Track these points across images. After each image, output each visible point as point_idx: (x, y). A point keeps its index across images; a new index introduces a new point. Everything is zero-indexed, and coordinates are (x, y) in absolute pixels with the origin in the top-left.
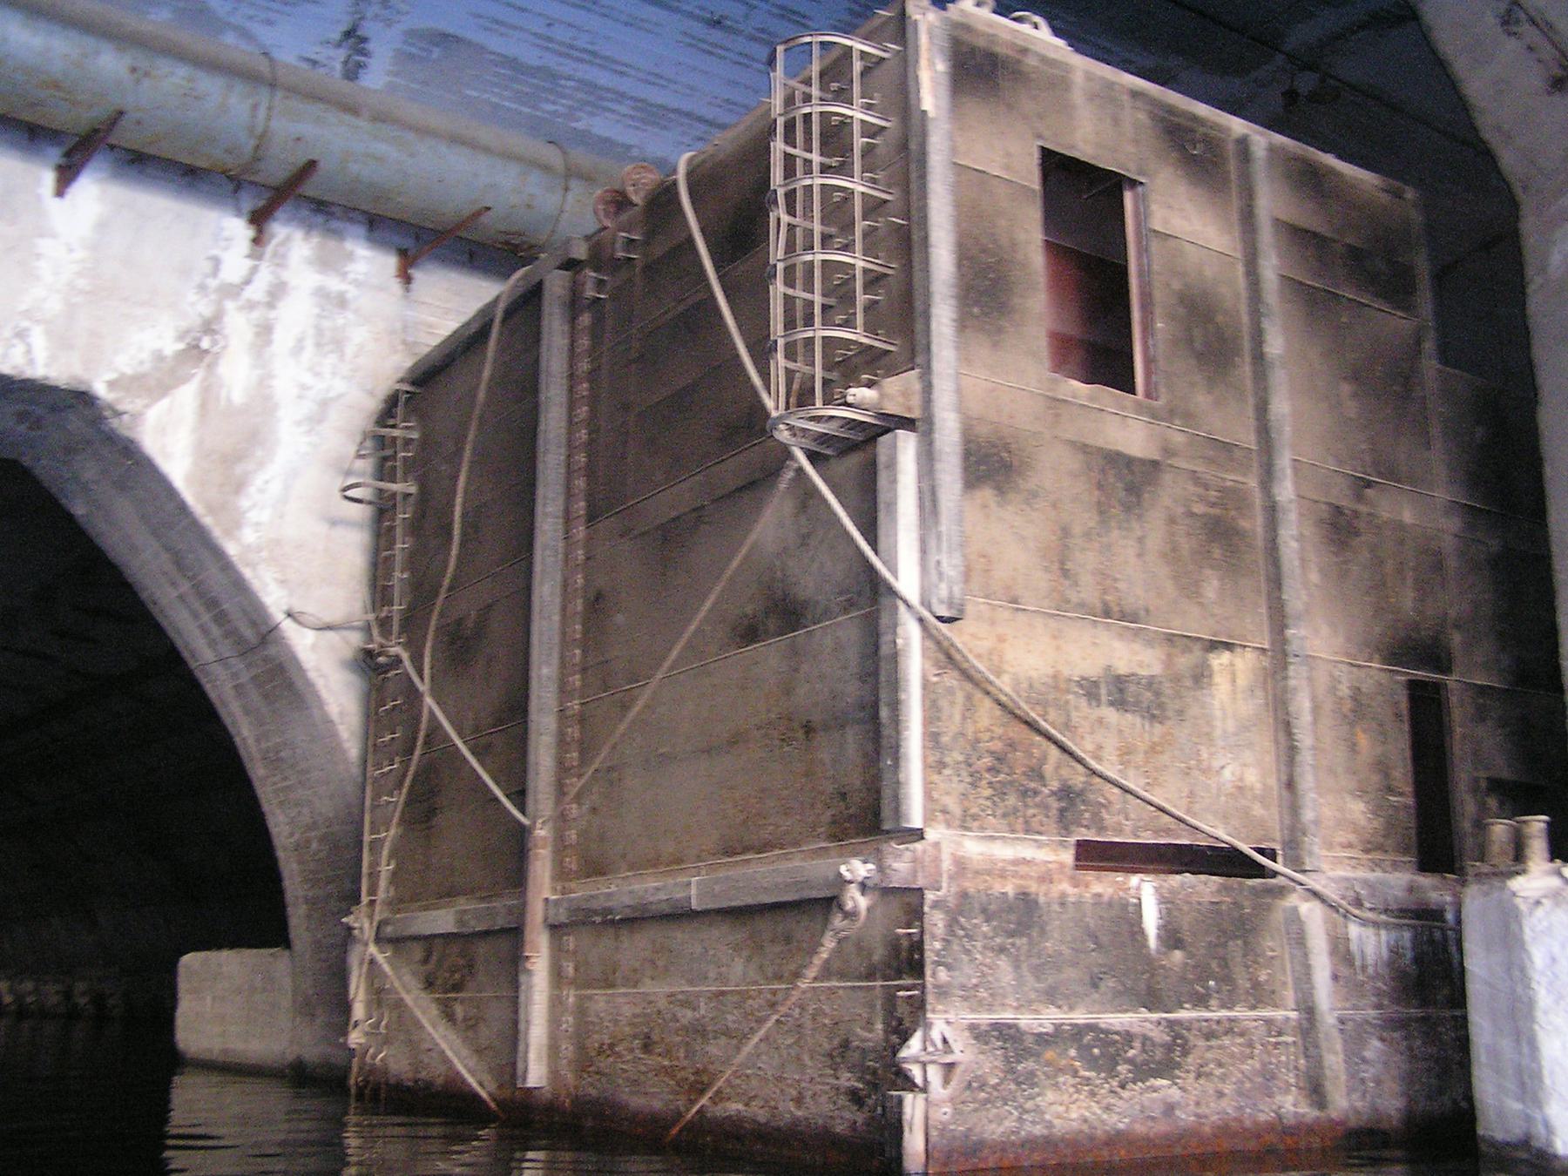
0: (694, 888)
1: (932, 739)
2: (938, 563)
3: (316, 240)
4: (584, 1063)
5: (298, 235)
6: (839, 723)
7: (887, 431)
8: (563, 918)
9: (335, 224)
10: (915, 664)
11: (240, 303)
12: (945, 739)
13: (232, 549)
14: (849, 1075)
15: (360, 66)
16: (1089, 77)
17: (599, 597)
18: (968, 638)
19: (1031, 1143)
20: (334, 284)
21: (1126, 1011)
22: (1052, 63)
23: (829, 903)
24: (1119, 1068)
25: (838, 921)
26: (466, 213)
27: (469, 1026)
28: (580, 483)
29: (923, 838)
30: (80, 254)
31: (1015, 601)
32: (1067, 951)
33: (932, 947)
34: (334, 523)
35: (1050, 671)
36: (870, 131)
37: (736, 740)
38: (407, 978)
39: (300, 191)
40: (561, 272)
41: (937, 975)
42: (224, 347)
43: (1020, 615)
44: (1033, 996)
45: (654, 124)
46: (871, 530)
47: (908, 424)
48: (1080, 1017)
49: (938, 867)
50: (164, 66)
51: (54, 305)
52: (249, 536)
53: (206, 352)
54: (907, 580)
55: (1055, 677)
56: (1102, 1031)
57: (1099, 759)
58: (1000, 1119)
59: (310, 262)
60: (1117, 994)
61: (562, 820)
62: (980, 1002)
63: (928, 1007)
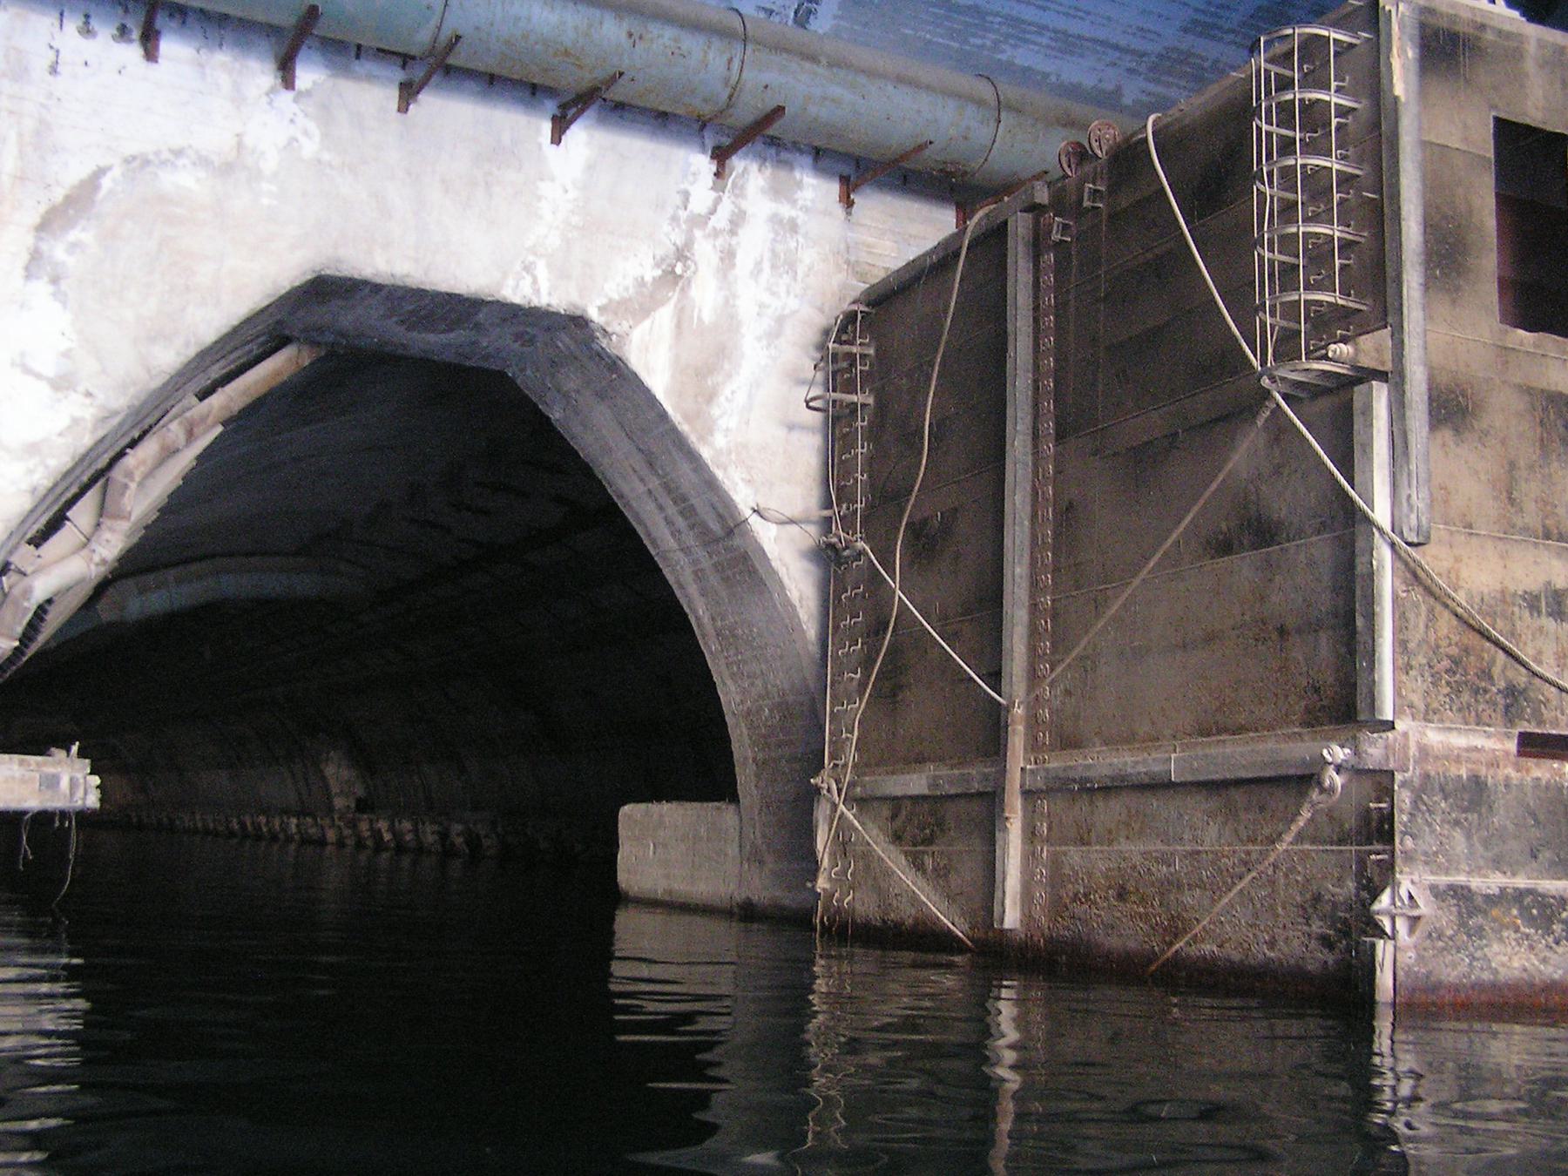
0: (1174, 762)
1: (1401, 645)
2: (1409, 496)
3: (768, 171)
4: (1057, 907)
5: (754, 167)
6: (1314, 627)
7: (1360, 381)
8: (1040, 784)
9: (785, 155)
10: (1387, 583)
11: (707, 231)
12: (1411, 645)
13: (706, 453)
14: (1321, 923)
15: (810, 12)
16: (1541, 44)
17: (1070, 507)
18: (1432, 560)
19: (1479, 986)
20: (786, 211)
21: (1559, 879)
22: (1508, 36)
23: (1306, 779)
24: (1554, 927)
25: (1315, 795)
26: (910, 144)
27: (940, 875)
28: (1049, 405)
29: (1394, 728)
30: (572, 194)
31: (1470, 526)
32: (1511, 827)
33: (1400, 819)
34: (791, 427)
35: (1498, 587)
36: (1343, 112)
37: (1210, 638)
38: (875, 832)
39: (770, 132)
40: (1025, 214)
41: (1403, 843)
42: (694, 273)
43: (1474, 540)
44: (1482, 862)
45: (1072, 53)
46: (1346, 462)
47: (1382, 376)
48: (1521, 882)
49: (1406, 754)
50: (654, 29)
51: (554, 241)
52: (720, 440)
53: (681, 277)
54: (1381, 513)
55: (1503, 592)
56: (1540, 895)
57: (1539, 663)
58: (1454, 965)
59: (763, 191)
60: (1552, 864)
61: (1034, 703)
62: (1439, 866)
63: (1397, 869)
